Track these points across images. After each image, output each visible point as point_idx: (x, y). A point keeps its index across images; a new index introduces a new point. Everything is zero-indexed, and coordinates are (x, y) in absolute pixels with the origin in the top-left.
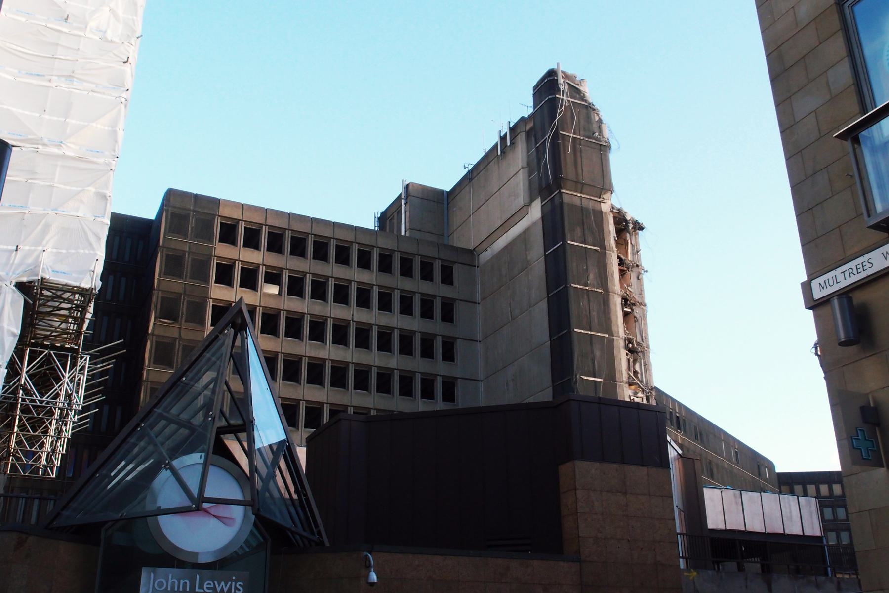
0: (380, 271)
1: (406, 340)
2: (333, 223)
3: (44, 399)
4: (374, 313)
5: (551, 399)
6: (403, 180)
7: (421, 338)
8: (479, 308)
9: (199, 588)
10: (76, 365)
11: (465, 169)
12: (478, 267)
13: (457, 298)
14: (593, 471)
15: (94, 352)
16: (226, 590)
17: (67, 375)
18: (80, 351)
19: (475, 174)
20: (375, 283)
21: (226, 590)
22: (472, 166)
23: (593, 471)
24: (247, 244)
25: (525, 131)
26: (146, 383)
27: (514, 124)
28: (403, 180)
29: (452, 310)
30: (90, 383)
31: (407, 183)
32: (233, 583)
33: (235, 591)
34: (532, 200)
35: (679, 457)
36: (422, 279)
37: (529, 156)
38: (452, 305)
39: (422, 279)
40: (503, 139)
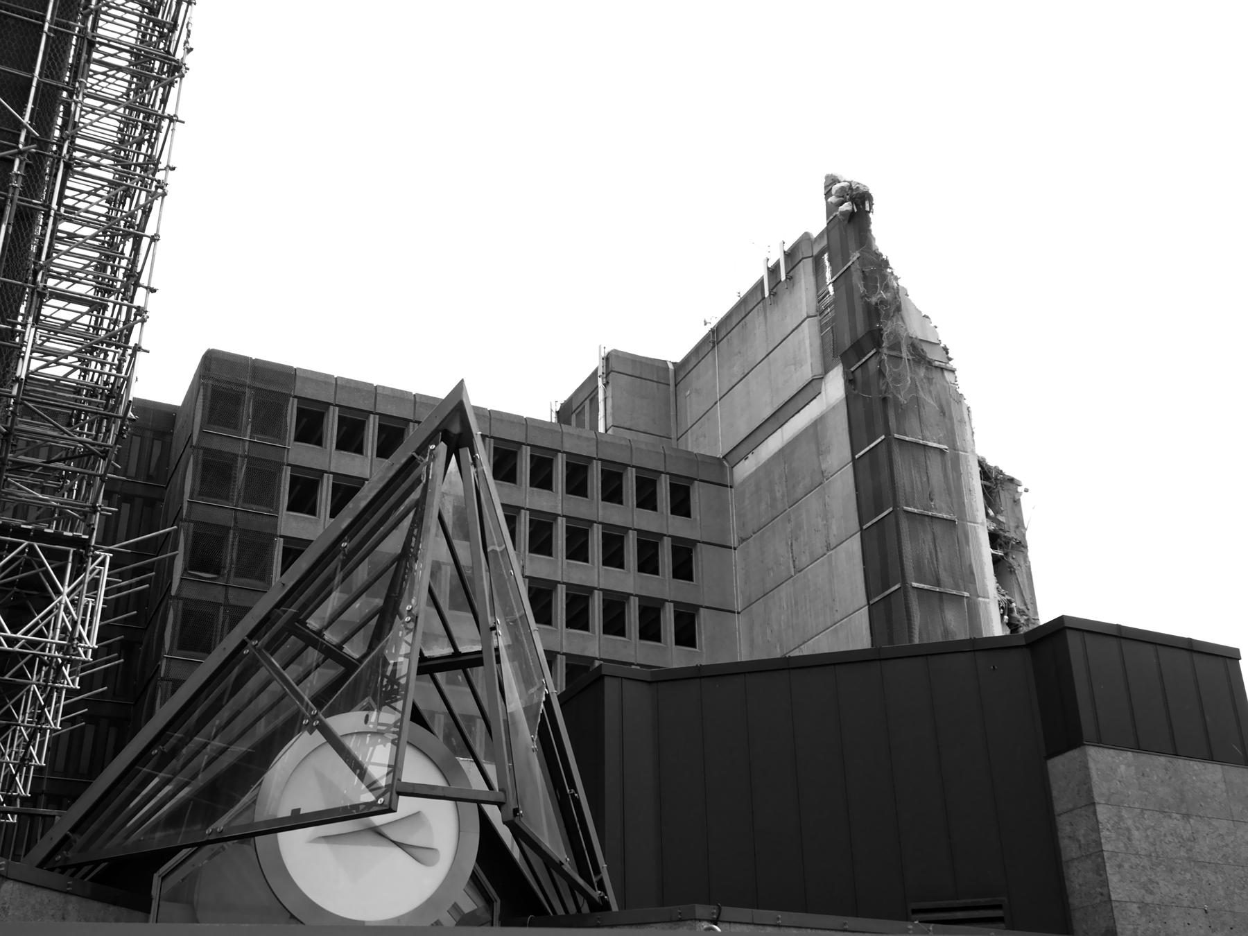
0: (568, 492)
1: (615, 606)
2: (489, 411)
3: (19, 635)
4: (560, 563)
6: (551, 403)
7: (639, 606)
8: (736, 556)
10: (85, 570)
11: (705, 324)
12: (731, 487)
13: (698, 538)
14: (1123, 767)
15: (119, 547)
17: (66, 590)
18: (93, 543)
19: (723, 333)
20: (560, 513)
23: (1123, 767)
24: (342, 445)
26: (165, 682)
30: (105, 622)
31: (607, 350)
34: (826, 370)
36: (639, 506)
38: (690, 551)
39: (639, 506)
40: (773, 271)
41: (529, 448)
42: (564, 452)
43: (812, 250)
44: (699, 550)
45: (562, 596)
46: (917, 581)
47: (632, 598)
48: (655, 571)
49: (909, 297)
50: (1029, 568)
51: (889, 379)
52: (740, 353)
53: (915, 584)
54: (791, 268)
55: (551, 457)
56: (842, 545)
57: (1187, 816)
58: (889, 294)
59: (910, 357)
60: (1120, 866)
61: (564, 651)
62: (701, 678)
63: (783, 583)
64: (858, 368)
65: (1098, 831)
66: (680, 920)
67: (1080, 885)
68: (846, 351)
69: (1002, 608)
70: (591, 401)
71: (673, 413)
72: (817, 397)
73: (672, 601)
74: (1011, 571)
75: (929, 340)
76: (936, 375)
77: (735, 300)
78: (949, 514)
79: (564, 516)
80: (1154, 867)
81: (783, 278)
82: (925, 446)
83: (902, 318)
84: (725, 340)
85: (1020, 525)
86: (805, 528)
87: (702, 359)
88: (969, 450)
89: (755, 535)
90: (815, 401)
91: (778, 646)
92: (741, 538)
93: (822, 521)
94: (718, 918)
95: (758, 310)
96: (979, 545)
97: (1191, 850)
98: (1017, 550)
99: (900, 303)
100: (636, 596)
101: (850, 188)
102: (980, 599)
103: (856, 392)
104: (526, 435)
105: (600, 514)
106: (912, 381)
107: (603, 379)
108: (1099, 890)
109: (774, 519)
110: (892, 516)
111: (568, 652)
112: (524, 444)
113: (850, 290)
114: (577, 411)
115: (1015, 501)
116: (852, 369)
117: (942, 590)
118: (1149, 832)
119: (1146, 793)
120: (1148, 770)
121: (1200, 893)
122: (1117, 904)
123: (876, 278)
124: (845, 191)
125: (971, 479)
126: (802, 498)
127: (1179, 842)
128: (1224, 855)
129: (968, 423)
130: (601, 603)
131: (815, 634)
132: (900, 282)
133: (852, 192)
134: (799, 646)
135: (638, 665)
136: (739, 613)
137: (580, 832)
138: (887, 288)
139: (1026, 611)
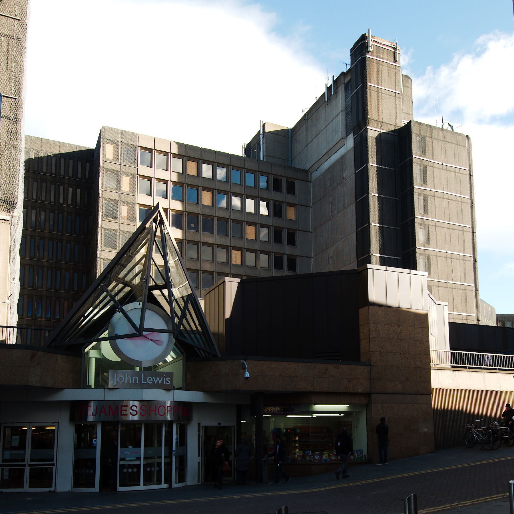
6: (261, 121)
8: (311, 210)
9: (144, 382)
12: (311, 182)
14: (380, 312)
16: (160, 382)
19: (309, 116)
21: (160, 382)
28: (261, 121)
32: (164, 378)
33: (165, 383)
34: (347, 134)
37: (346, 102)
40: (329, 89)
52: (315, 125)
57: (399, 326)
77: (315, 101)
81: (333, 94)
93: (343, 197)
95: (323, 106)
97: (399, 336)
107: (262, 135)
108: (367, 348)
111: (247, 248)
114: (253, 149)
119: (387, 319)
120: (389, 312)
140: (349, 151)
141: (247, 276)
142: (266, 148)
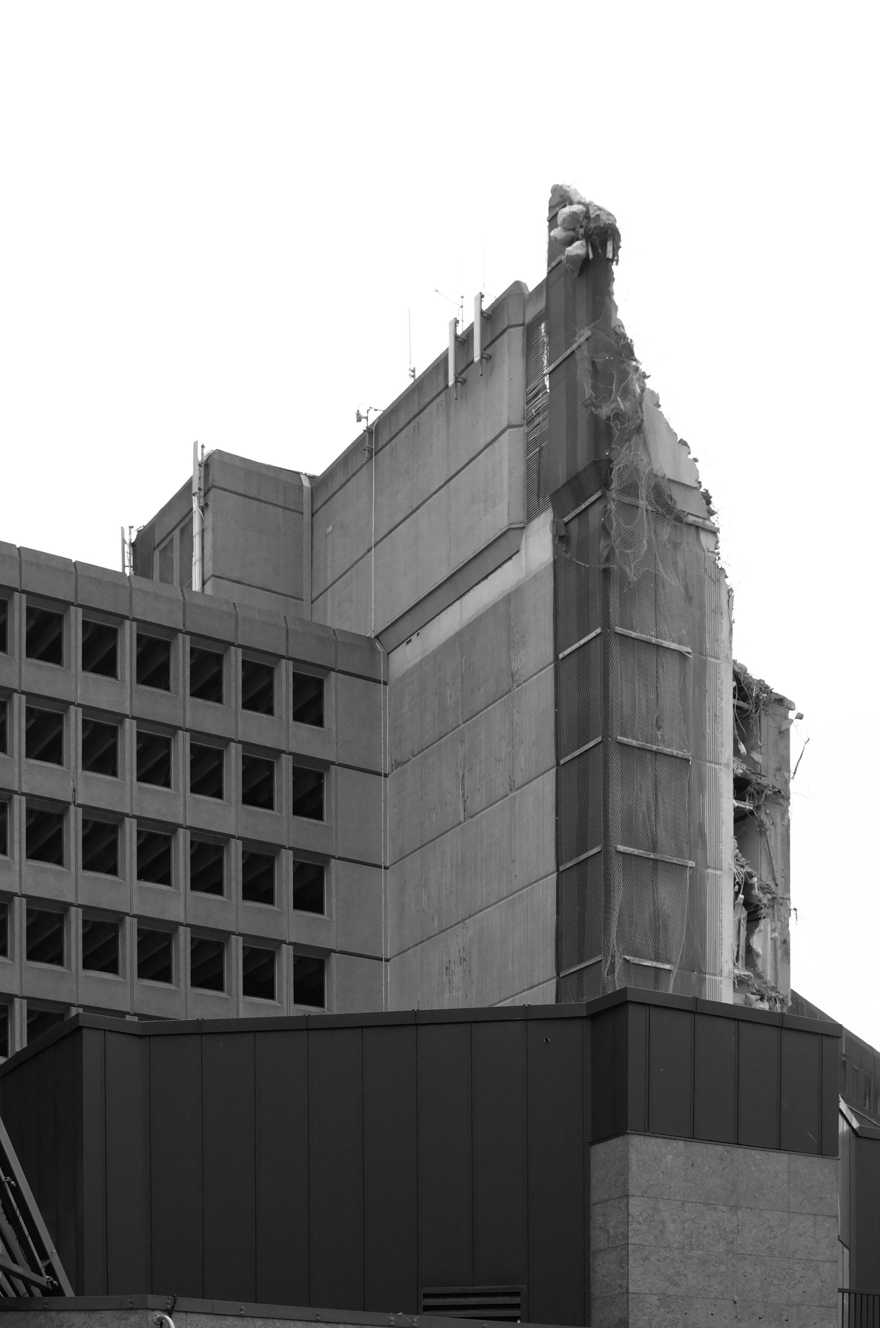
2: (19, 549)
4: (128, 788)
5: (551, 1000)
6: (122, 529)
7: (244, 853)
8: (387, 786)
11: (359, 419)
12: (385, 683)
14: (669, 1157)
19: (385, 437)
20: (128, 712)
22: (379, 413)
25: (523, 325)
27: (493, 300)
28: (196, 444)
29: (319, 788)
31: (207, 451)
34: (530, 516)
35: (852, 1135)
38: (320, 777)
40: (463, 342)
41: (80, 610)
42: (134, 620)
43: (524, 313)
44: (333, 775)
45: (131, 835)
46: (624, 844)
47: (233, 841)
48: (268, 804)
49: (660, 409)
50: (787, 828)
51: (616, 542)
53: (621, 848)
54: (489, 341)
55: (116, 627)
56: (530, 784)
57: (735, 1208)
58: (628, 404)
59: (649, 508)
60: (646, 1259)
61: (135, 912)
62: (201, 1034)
63: (448, 831)
64: (575, 517)
65: (627, 1224)
66: (131, 1309)
67: (603, 1276)
68: (558, 490)
69: (738, 883)
70: (182, 531)
71: (306, 560)
72: (514, 558)
73: (290, 848)
74: (760, 831)
75: (682, 482)
76: (688, 536)
78: (681, 749)
79: (133, 718)
80: (685, 1260)
81: (477, 358)
82: (658, 647)
83: (645, 443)
84: (387, 448)
85: (783, 766)
86: (483, 754)
87: (354, 475)
88: (722, 655)
89: (414, 758)
90: (510, 563)
91: (436, 918)
92: (395, 761)
94: (173, 1307)
96: (717, 795)
98: (772, 802)
99: (642, 420)
100: (239, 838)
101: (587, 215)
102: (710, 871)
103: (568, 556)
104: (76, 589)
105: (187, 718)
106: (648, 547)
107: (199, 498)
108: (619, 1282)
109: (441, 738)
110: (600, 748)
111: (141, 913)
112: (72, 604)
113: (572, 391)
114: (161, 547)
115: (781, 732)
116: (566, 519)
117: (658, 857)
118: (686, 1225)
121: (733, 1284)
122: (635, 1296)
123: (612, 375)
124: (578, 221)
125: (719, 699)
126: (482, 710)
127: (720, 1235)
128: (769, 1247)
129: (725, 615)
130: (188, 846)
131: (485, 905)
132: (649, 384)
133: (588, 223)
134: (463, 921)
135: (135, 1015)
136: (386, 868)
137: (21, 1219)
138: (626, 392)
139: (773, 886)
140: (535, 576)
141: (141, 1016)
142: (214, 546)
